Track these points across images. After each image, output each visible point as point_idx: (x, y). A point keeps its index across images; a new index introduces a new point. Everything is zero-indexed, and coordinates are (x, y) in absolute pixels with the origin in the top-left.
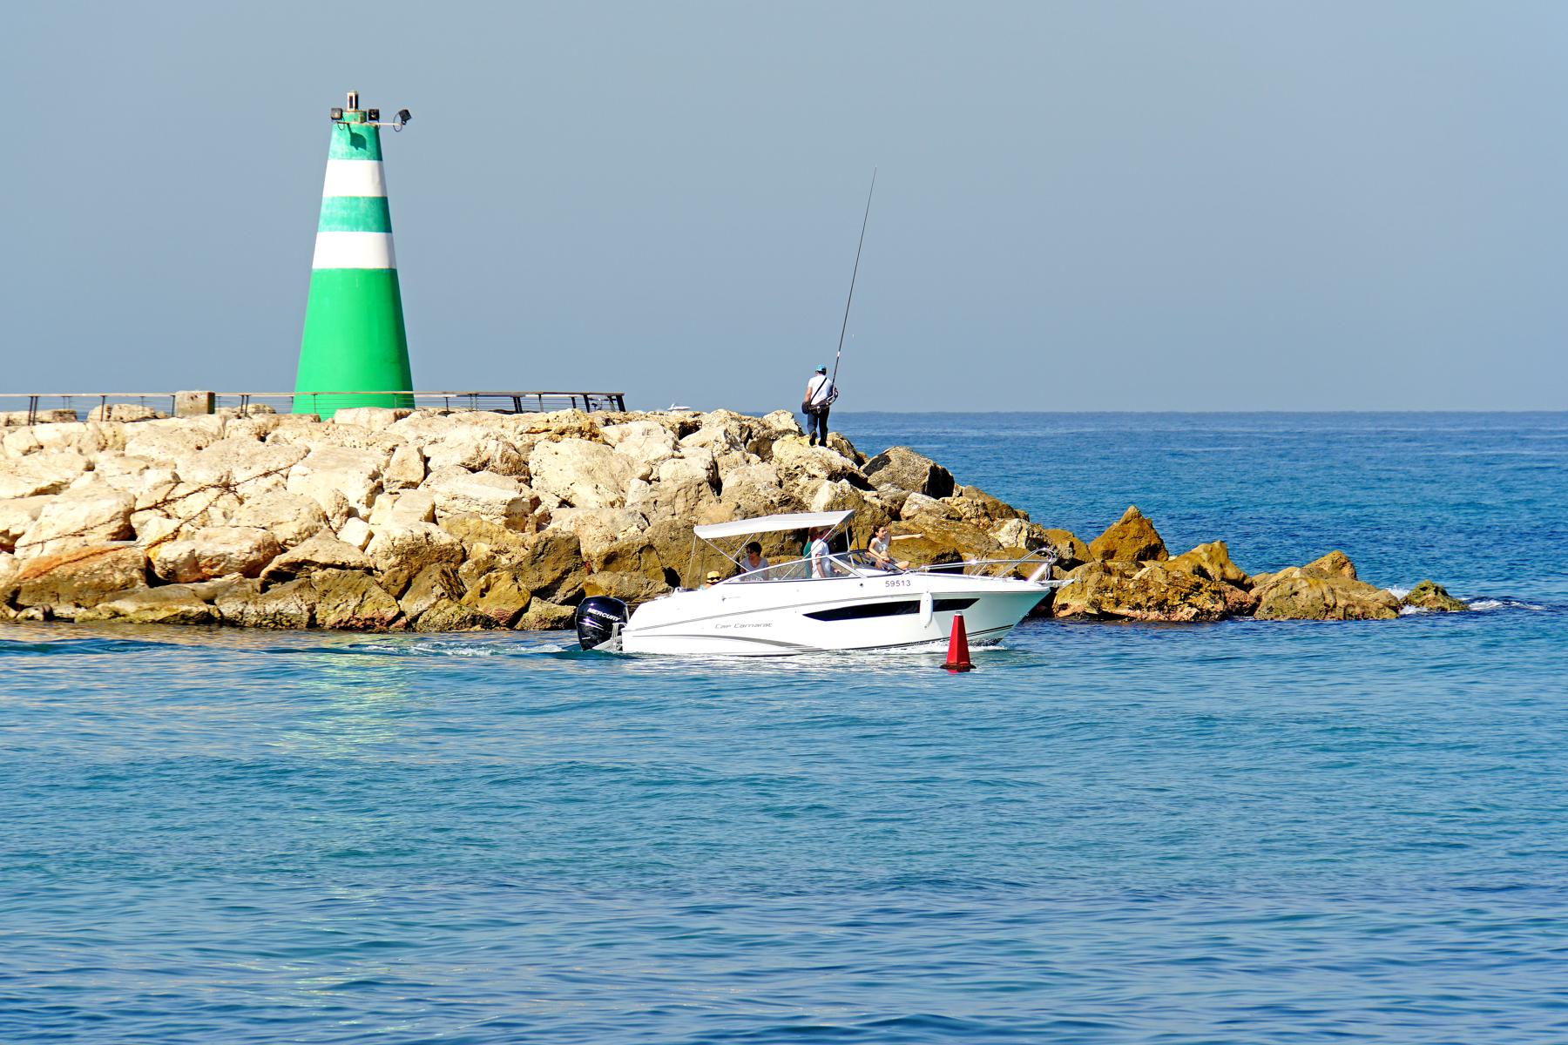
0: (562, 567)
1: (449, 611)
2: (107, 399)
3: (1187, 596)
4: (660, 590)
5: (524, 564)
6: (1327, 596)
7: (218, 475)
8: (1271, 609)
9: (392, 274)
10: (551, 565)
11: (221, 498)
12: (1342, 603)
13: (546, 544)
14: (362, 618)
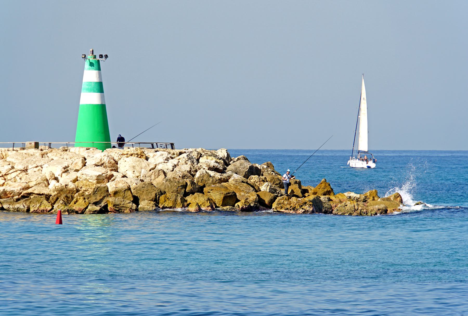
0: (103, 195)
1: (62, 208)
2: (15, 144)
3: (302, 206)
4: (128, 202)
5: (91, 194)
6: (355, 206)
7: (24, 167)
8: (337, 210)
9: (103, 107)
10: (99, 195)
11: (21, 174)
12: (360, 208)
13: (98, 188)
14: (41, 210)
